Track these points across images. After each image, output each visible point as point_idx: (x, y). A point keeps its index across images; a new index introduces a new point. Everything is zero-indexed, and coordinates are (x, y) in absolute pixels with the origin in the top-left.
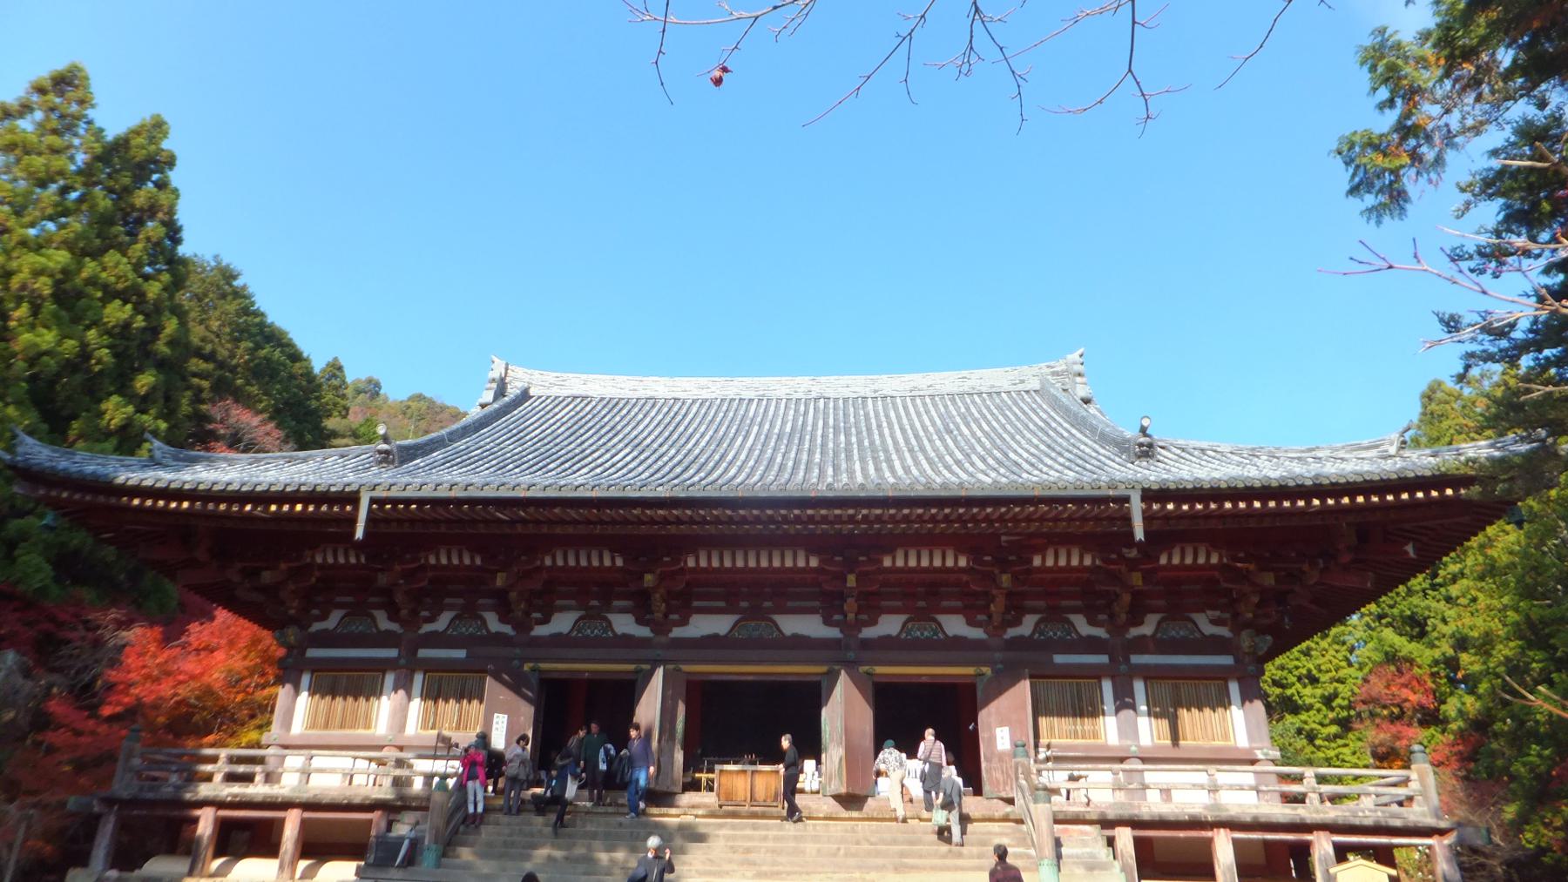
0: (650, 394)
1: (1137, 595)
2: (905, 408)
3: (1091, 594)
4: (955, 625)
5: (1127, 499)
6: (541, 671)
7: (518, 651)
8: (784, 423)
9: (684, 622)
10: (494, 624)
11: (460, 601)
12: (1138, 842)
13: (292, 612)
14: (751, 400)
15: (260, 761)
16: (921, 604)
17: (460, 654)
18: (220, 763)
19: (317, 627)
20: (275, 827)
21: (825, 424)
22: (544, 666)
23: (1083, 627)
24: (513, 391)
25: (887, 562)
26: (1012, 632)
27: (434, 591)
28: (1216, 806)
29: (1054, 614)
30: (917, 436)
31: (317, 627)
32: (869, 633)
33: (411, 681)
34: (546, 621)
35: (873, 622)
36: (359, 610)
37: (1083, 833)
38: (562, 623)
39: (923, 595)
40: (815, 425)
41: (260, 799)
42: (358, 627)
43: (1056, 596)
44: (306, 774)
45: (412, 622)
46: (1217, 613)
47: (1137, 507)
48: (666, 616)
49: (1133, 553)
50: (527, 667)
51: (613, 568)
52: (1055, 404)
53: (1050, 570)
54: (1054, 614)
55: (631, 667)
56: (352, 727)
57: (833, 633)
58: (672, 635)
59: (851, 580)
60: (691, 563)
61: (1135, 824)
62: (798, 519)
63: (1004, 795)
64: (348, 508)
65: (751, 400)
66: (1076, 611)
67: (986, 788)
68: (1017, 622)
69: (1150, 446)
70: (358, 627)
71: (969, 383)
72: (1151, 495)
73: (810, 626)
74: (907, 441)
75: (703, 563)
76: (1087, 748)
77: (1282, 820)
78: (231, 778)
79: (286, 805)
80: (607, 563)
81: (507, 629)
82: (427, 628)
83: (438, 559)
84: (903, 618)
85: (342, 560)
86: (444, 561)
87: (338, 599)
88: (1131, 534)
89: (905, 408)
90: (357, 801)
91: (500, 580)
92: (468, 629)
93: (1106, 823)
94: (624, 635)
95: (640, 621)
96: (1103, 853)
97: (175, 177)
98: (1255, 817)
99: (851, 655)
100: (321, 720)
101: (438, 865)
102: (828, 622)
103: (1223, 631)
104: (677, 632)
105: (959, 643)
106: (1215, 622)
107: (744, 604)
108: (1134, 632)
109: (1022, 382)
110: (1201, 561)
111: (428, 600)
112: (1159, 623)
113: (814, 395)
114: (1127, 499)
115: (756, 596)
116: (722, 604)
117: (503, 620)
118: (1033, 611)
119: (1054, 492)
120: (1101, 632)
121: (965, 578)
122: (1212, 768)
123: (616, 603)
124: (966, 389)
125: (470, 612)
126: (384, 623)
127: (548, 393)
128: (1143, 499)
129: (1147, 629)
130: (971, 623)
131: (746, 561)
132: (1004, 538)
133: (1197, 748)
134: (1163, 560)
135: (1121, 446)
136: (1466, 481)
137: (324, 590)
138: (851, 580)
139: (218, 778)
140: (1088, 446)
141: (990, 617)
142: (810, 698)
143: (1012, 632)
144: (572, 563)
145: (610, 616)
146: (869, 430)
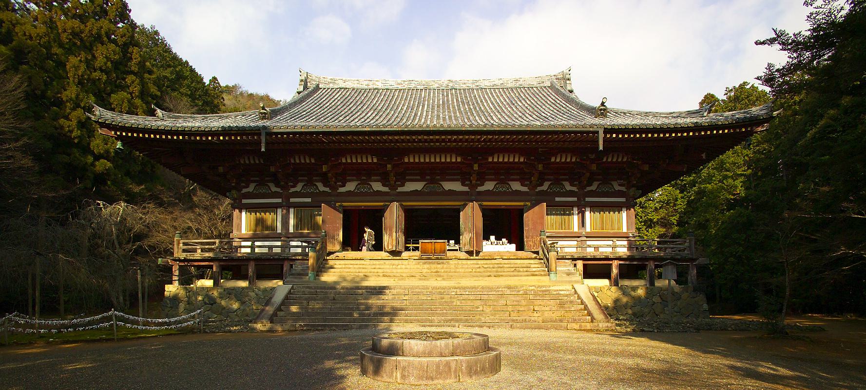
1: (541, 173)
2: (492, 94)
3: (572, 173)
4: (516, 186)
5: (597, 132)
8: (439, 100)
9: (403, 185)
10: (321, 188)
12: (585, 266)
17: (309, 200)
19: (244, 191)
21: (457, 100)
22: (344, 204)
23: (568, 187)
24: (311, 86)
25: (490, 160)
26: (539, 189)
27: (295, 174)
28: (615, 253)
29: (557, 182)
30: (499, 106)
31: (244, 191)
32: (481, 189)
36: (261, 183)
39: (503, 173)
40: (453, 100)
42: (263, 190)
43: (558, 174)
45: (285, 188)
47: (601, 135)
49: (593, 156)
52: (557, 92)
53: (495, 163)
54: (557, 182)
57: (466, 189)
59: (476, 167)
60: (406, 160)
61: (583, 259)
62: (455, 141)
66: (566, 180)
67: (526, 248)
68: (541, 185)
69: (604, 110)
70: (263, 190)
72: (607, 131)
74: (495, 107)
81: (327, 189)
82: (292, 190)
84: (495, 183)
85: (252, 162)
86: (298, 161)
88: (598, 148)
89: (492, 94)
91: (325, 168)
93: (574, 259)
96: (572, 268)
97: (190, 64)
102: (463, 184)
103: (623, 189)
104: (400, 189)
105: (518, 193)
108: (589, 189)
110: (568, 160)
114: (597, 132)
115: (433, 174)
119: (567, 129)
120: (575, 189)
121: (522, 166)
122: (615, 240)
125: (310, 183)
126: (274, 189)
128: (604, 132)
129: (593, 187)
135: (591, 111)
136: (723, 127)
138: (476, 167)
140: (575, 111)
141: (531, 182)
142: (454, 215)
143: (539, 189)
146: (477, 103)
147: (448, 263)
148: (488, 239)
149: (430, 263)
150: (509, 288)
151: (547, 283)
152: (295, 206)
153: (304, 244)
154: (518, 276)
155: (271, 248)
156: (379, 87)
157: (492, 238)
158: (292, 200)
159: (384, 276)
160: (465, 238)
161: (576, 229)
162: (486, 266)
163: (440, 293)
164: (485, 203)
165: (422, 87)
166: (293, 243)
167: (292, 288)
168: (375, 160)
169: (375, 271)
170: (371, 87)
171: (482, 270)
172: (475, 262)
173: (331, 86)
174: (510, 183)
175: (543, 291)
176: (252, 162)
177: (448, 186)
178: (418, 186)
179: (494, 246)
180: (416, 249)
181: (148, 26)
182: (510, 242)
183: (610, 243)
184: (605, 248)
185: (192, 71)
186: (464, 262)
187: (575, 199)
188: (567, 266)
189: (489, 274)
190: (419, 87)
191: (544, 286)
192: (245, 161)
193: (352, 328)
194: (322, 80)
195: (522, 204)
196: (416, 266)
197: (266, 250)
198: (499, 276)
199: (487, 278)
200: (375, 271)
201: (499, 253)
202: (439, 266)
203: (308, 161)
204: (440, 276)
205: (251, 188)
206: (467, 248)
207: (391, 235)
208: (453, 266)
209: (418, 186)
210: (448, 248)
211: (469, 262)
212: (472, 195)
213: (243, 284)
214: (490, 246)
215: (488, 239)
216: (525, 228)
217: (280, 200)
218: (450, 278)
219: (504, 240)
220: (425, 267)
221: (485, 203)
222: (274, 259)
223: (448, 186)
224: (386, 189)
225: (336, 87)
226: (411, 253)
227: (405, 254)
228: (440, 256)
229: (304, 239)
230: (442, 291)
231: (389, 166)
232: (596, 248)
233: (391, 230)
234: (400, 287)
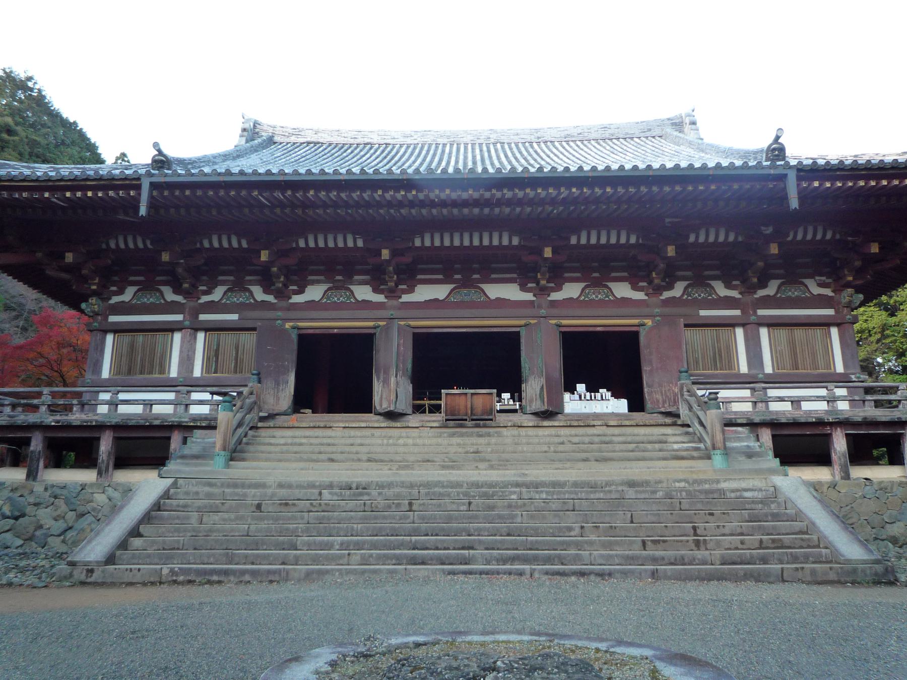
0: (367, 140)
4: (622, 290)
6: (299, 329)
7: (280, 314)
9: (411, 290)
10: (259, 294)
11: (232, 278)
13: (94, 287)
14: (444, 145)
15: (79, 395)
17: (235, 317)
18: (43, 398)
19: (115, 299)
20: (94, 443)
22: (301, 324)
23: (721, 290)
26: (666, 295)
28: (834, 411)
31: (115, 299)
33: (195, 338)
34: (301, 291)
35: (559, 288)
37: (736, 432)
38: (314, 293)
41: (79, 423)
44: (113, 404)
46: (824, 278)
50: (288, 325)
51: (356, 248)
55: (371, 324)
56: (151, 373)
57: (529, 296)
58: (291, 301)
59: (548, 253)
60: (418, 243)
63: (663, 410)
64: (132, 193)
65: (444, 145)
66: (715, 278)
67: (649, 405)
68: (670, 287)
71: (610, 131)
75: (428, 243)
76: (725, 376)
77: (884, 419)
78: (52, 409)
79: (101, 427)
81: (270, 298)
84: (583, 285)
87: (132, 278)
90: (157, 422)
92: (239, 298)
95: (376, 290)
98: (794, 419)
99: (543, 312)
100: (125, 368)
101: (227, 466)
102: (523, 288)
103: (828, 292)
104: (405, 298)
106: (821, 285)
108: (761, 293)
109: (650, 130)
110: (819, 237)
111: (205, 278)
112: (583, 290)
113: (492, 140)
116: (441, 277)
117: (266, 291)
118: (683, 279)
123: (356, 277)
124: (607, 136)
126: (170, 296)
127: (288, 140)
128: (799, 179)
130: (635, 288)
132: (667, 220)
133: (808, 375)
137: (116, 272)
138: (548, 253)
139: (43, 409)
145: (352, 287)
147: (499, 435)
148: (572, 390)
149: (462, 435)
150: (632, 484)
151: (710, 476)
152: (208, 328)
153: (216, 397)
154: (644, 459)
155: (149, 404)
156: (375, 141)
157: (581, 388)
158: (202, 317)
159: (369, 460)
160: (533, 387)
161: (744, 368)
162: (576, 440)
163: (486, 496)
165: (445, 141)
166: (195, 396)
167: (175, 485)
168: (360, 243)
169: (354, 449)
170: (358, 141)
171: (568, 447)
172: (553, 431)
173: (293, 139)
174: (610, 284)
175: (707, 492)
176: (131, 245)
177: (495, 291)
179: (584, 403)
180: (436, 409)
181: (93, 141)
182: (617, 395)
183: (823, 392)
184: (814, 403)
185: (82, 135)
186: (531, 432)
187: (737, 312)
188: (742, 439)
189: (584, 455)
190: (441, 141)
191: (706, 481)
192: (118, 243)
193: (285, 577)
194: (278, 131)
196: (434, 441)
197: (138, 409)
198: (606, 460)
199: (581, 465)
200: (354, 449)
201: (596, 416)
202: (482, 441)
204: (483, 460)
205: (127, 296)
206: (537, 406)
207: (386, 382)
208: (509, 440)
209: (440, 292)
210: (498, 406)
211: (540, 432)
212: (540, 307)
213: (87, 476)
214: (577, 403)
215: (572, 390)
216: (646, 368)
217: (179, 317)
218: (503, 464)
219: (603, 391)
220: (457, 442)
222: (152, 427)
224: (380, 298)
225: (302, 140)
226: (427, 417)
227: (414, 420)
228: (483, 419)
229: (215, 389)
230: (489, 491)
231: (385, 254)
232: (796, 402)
233: (387, 372)
234: (402, 484)
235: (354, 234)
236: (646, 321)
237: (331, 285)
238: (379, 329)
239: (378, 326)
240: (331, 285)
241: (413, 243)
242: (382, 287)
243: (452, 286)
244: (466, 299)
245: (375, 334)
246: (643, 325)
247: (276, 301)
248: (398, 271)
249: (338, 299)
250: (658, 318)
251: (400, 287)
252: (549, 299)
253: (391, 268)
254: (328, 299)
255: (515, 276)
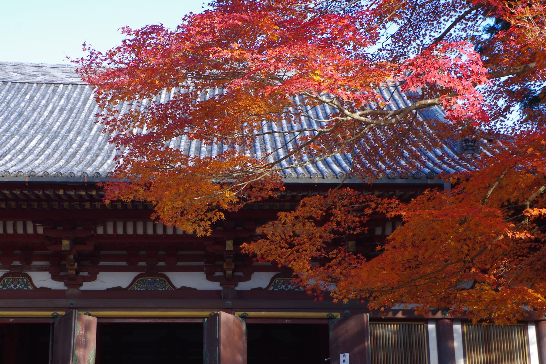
9: (92, 278)
16: (17, 263)
35: (247, 278)
48: (77, 272)
55: (49, 313)
57: (215, 286)
58: (82, 288)
60: (100, 231)
73: (196, 281)
75: (110, 231)
80: (30, 230)
83: (105, 230)
84: (271, 275)
94: (42, 288)
95: (55, 278)
102: (210, 277)
104: (87, 286)
107: (142, 264)
112: (272, 280)
116: (124, 264)
123: (35, 263)
131: (145, 229)
134: (100, 231)
144: (20, 231)
145: (31, 274)
164: (252, 314)
177: (180, 280)
178: (122, 280)
195: (324, 314)
203: (30, 230)
209: (122, 280)
221: (252, 314)
223: (180, 280)
224: (59, 286)
231: (66, 243)
235: (34, 222)
236: (335, 314)
237: (8, 271)
238: (57, 320)
239: (58, 316)
240: (8, 271)
241: (95, 231)
242: (62, 274)
243: (134, 274)
244: (151, 287)
245: (53, 324)
246: (333, 318)
247: (66, 288)
248: (80, 258)
249: (15, 286)
250: (347, 311)
251: (82, 274)
252: (237, 288)
253: (72, 257)
254: (276, 286)
255: (202, 263)
